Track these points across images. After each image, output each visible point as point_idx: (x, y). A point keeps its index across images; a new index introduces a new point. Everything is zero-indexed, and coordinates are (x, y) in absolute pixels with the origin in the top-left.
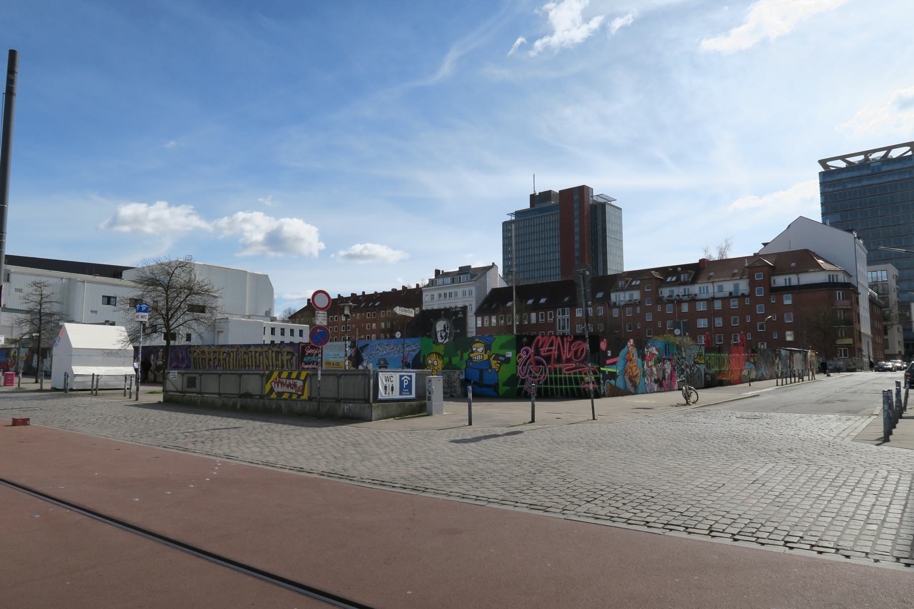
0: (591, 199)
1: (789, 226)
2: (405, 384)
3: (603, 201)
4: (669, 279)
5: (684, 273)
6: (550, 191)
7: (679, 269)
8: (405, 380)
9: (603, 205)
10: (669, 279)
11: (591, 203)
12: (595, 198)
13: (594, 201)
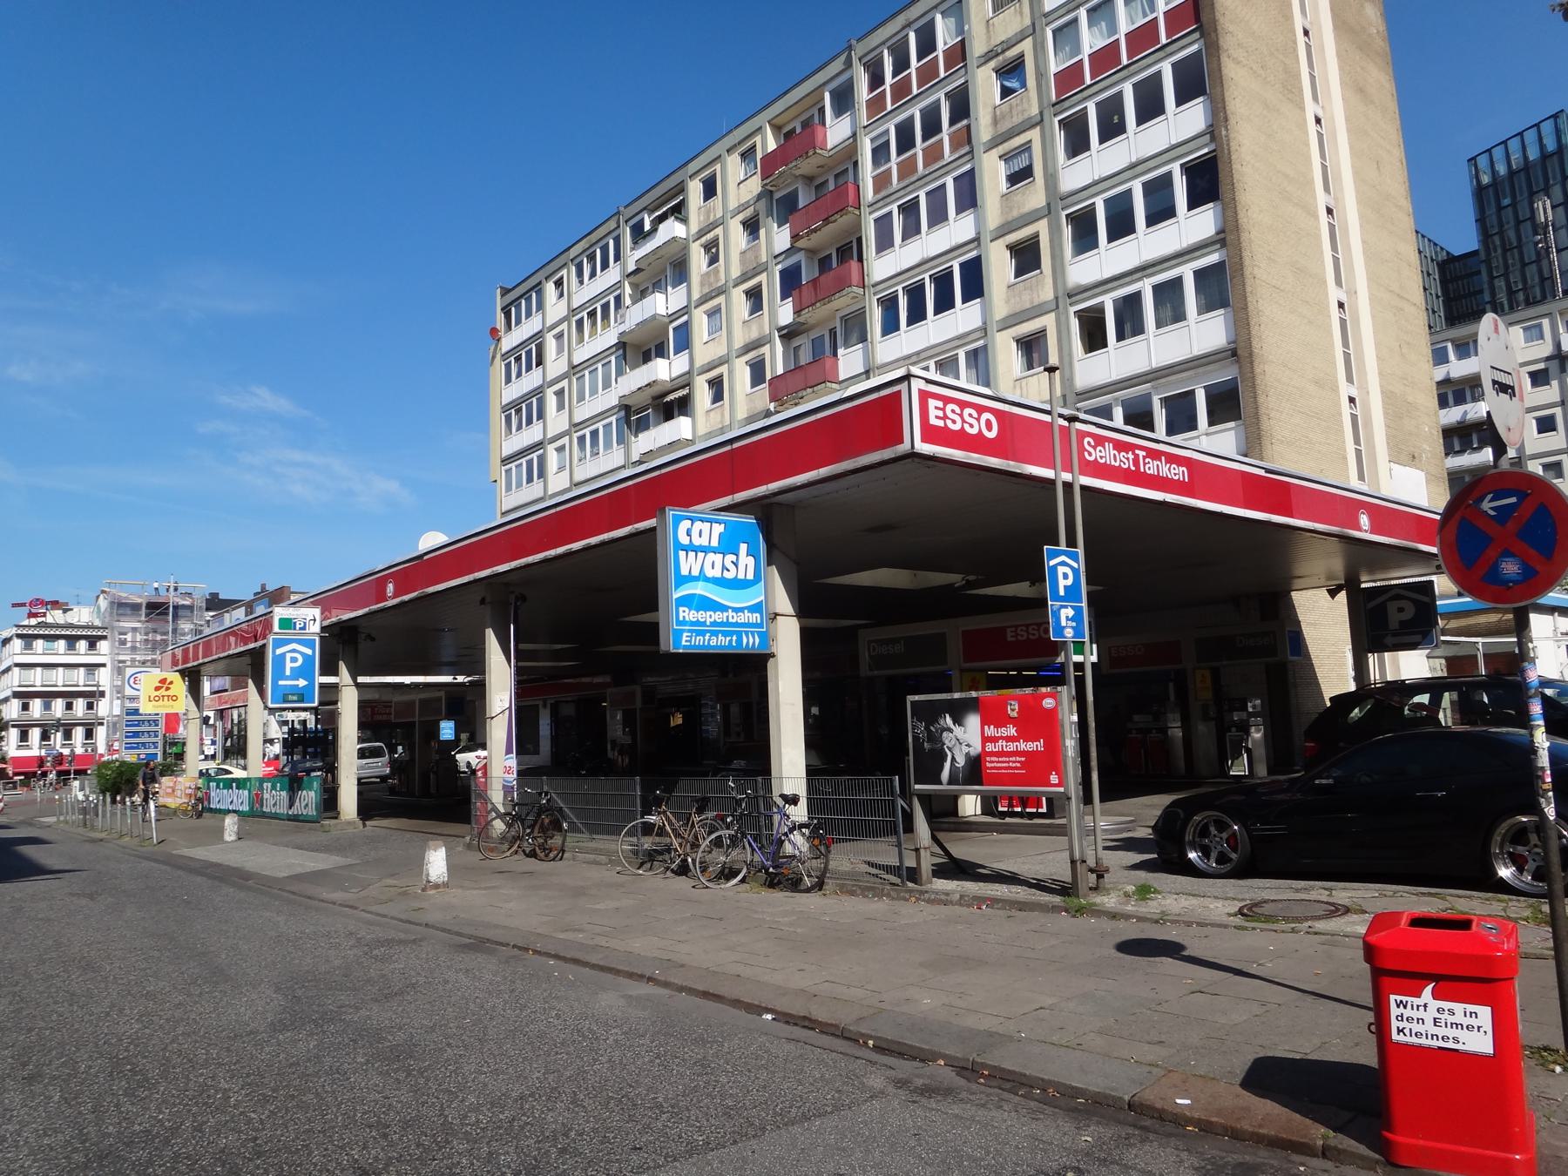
2: (289, 665)
8: (289, 656)
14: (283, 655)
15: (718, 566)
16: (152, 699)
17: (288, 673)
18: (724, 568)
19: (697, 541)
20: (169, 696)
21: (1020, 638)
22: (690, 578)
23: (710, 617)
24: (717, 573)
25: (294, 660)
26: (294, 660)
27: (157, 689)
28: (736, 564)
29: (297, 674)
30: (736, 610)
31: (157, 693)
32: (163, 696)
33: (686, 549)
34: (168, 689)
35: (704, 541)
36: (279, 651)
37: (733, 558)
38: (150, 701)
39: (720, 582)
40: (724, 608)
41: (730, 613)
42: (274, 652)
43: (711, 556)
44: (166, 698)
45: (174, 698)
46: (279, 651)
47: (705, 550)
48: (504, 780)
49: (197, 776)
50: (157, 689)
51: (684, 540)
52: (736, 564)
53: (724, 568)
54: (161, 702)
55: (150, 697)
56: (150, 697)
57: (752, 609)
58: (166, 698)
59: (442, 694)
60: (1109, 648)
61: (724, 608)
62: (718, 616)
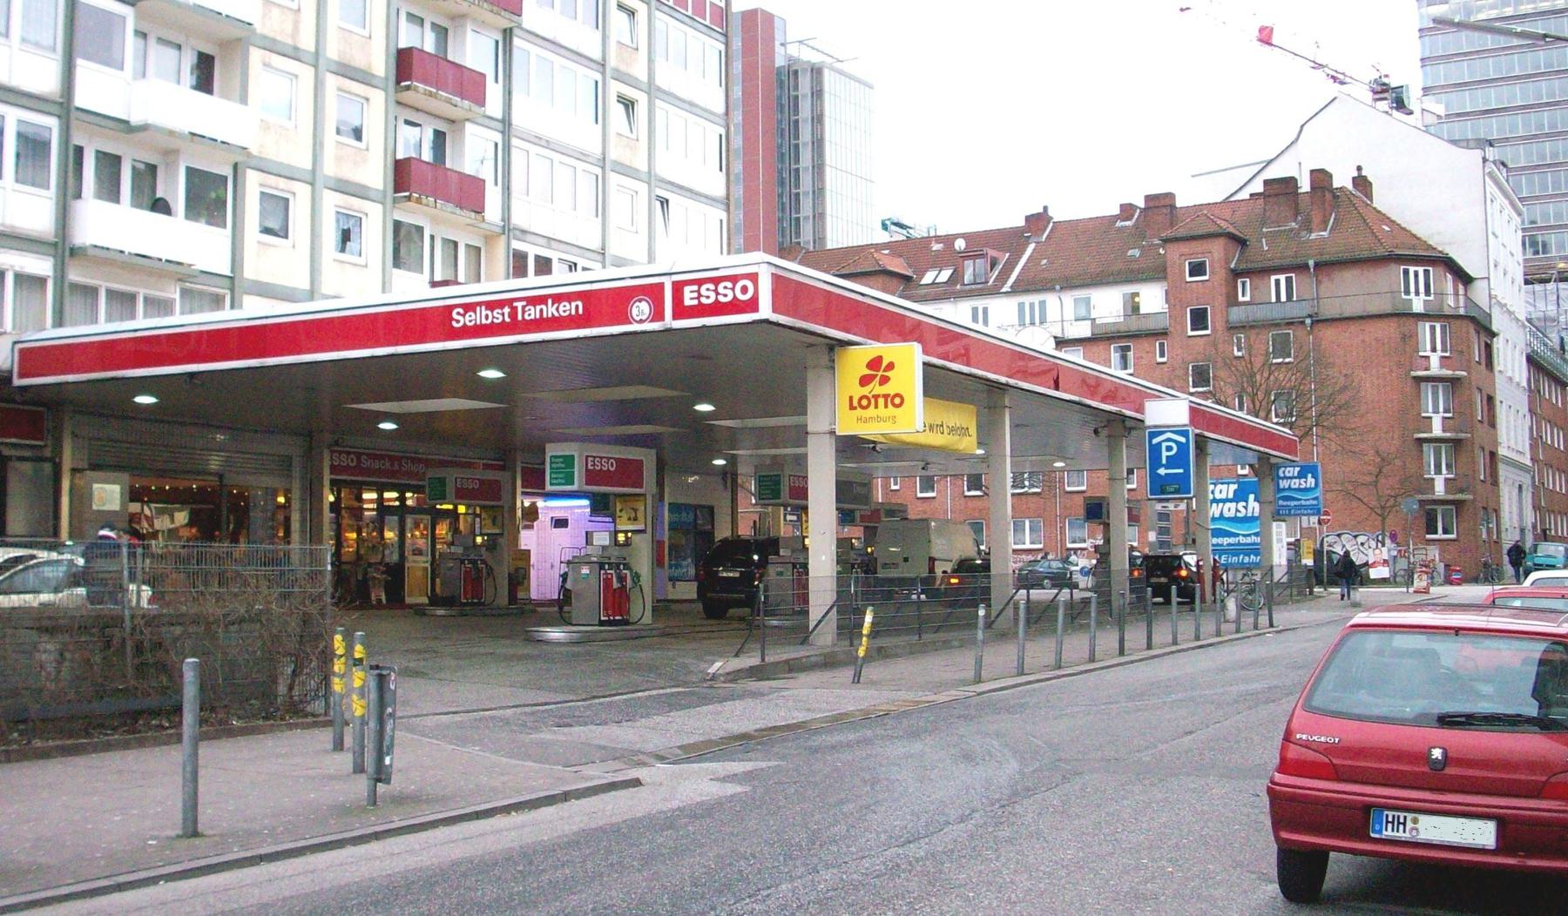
0: (779, 50)
1: (1302, 126)
2: (1165, 454)
3: (815, 58)
4: (929, 278)
5: (974, 257)
6: (1371, 184)
7: (960, 244)
8: (1164, 445)
9: (817, 72)
10: (929, 278)
11: (780, 62)
12: (793, 50)
13: (790, 58)
14: (1160, 444)
15: (1233, 510)
16: (855, 403)
17: (1164, 461)
18: (1237, 510)
19: (1287, 475)
20: (886, 396)
21: (704, 300)
22: (1284, 489)
23: (1226, 541)
24: (1297, 486)
25: (1169, 449)
26: (1169, 449)
27: (865, 381)
28: (1246, 508)
29: (1172, 462)
30: (1244, 536)
31: (866, 391)
32: (876, 397)
33: (1283, 478)
34: (884, 380)
35: (1291, 475)
36: (1155, 441)
37: (1244, 504)
38: (852, 408)
39: (1234, 520)
40: (1236, 535)
41: (1241, 538)
42: (1150, 442)
43: (1228, 505)
44: (881, 401)
45: (896, 400)
46: (1155, 441)
47: (1224, 501)
48: (1273, 782)
49: (1421, 93)
50: (865, 381)
51: (1282, 475)
52: (1246, 508)
53: (1237, 510)
54: (871, 412)
55: (851, 398)
56: (851, 398)
57: (1256, 534)
58: (881, 401)
59: (549, 488)
60: (587, 457)
61: (1236, 535)
62: (1232, 540)
